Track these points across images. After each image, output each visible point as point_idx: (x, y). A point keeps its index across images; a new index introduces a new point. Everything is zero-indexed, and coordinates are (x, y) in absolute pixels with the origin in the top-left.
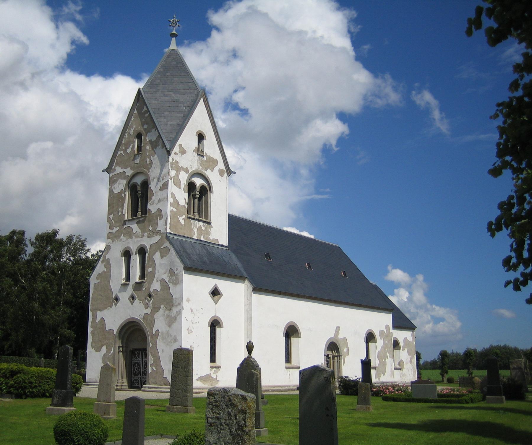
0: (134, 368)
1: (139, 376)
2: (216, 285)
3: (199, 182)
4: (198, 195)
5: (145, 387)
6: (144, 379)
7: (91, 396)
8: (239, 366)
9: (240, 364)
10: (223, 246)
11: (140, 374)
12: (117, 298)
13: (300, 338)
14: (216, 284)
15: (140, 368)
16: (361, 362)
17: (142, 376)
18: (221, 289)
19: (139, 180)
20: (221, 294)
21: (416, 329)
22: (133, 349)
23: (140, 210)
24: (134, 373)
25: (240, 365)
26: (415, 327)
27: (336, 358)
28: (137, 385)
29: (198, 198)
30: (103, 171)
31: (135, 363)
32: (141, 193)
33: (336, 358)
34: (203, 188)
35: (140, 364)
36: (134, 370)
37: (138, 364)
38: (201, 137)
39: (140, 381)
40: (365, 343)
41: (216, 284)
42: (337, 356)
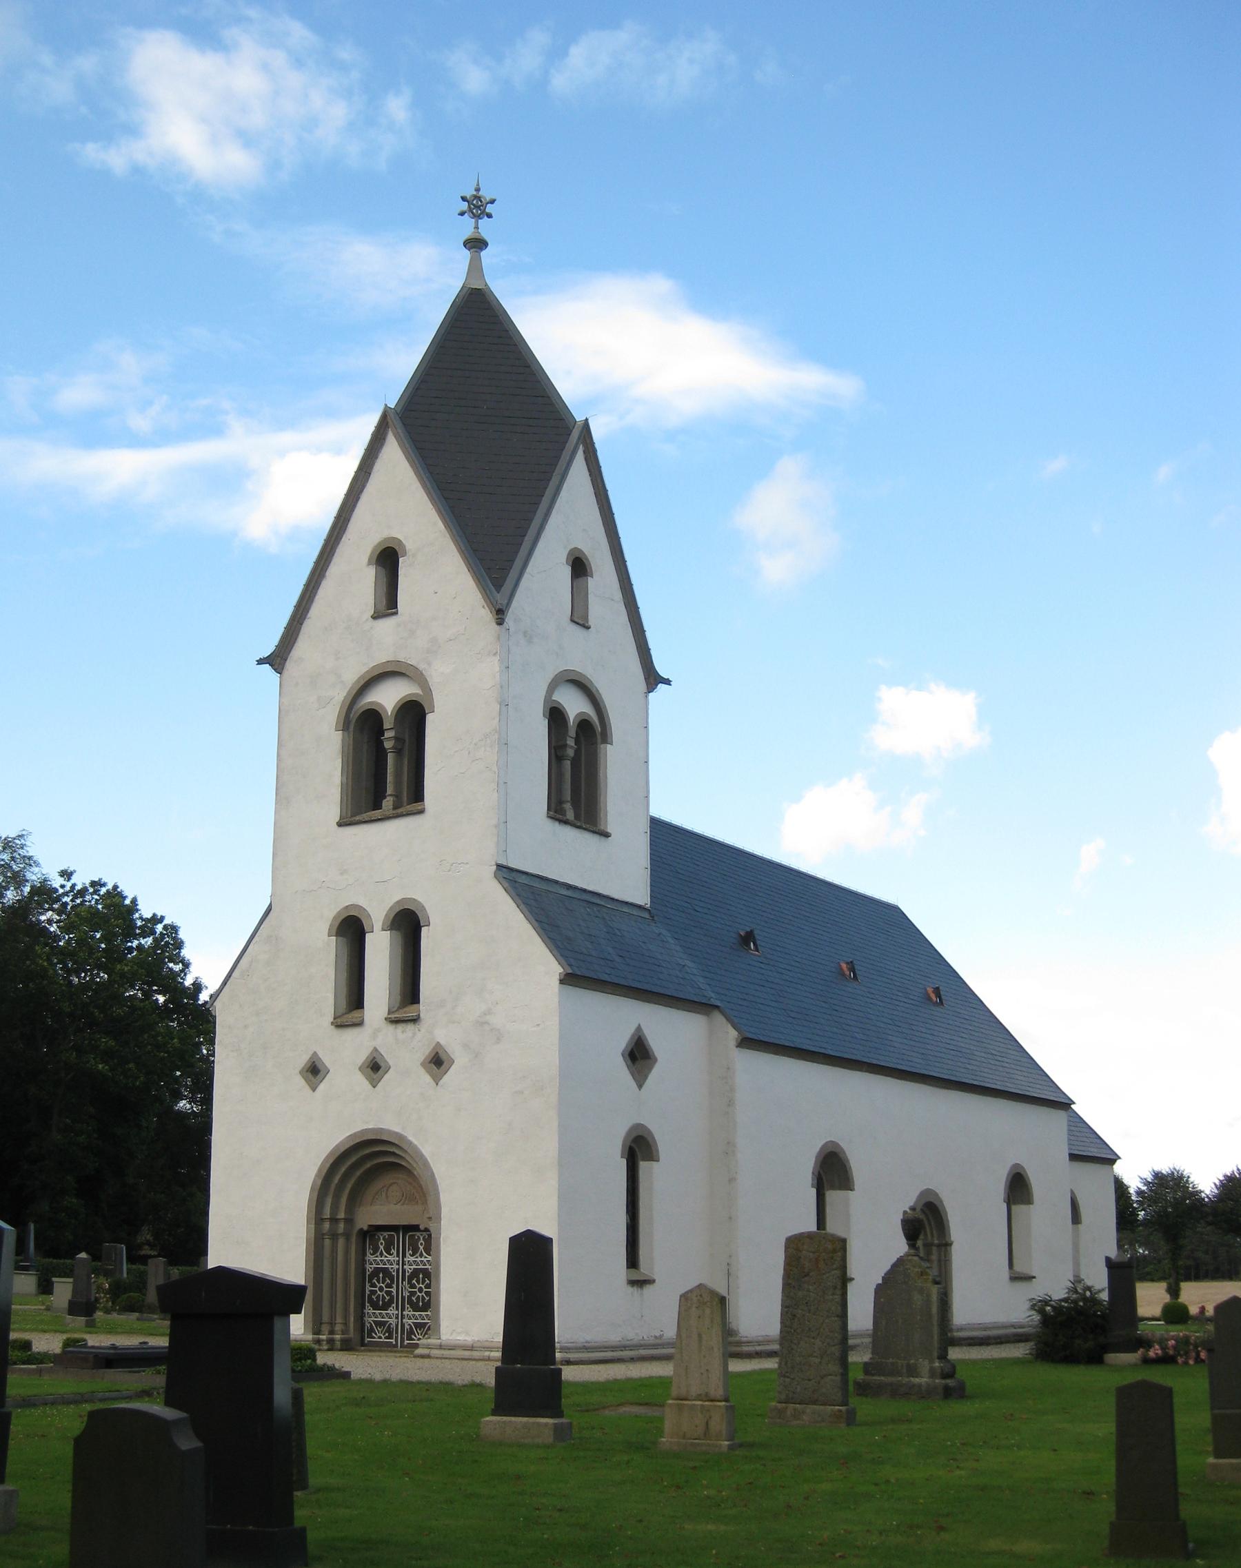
0: (373, 1285)
1: (392, 1311)
2: (641, 1029)
3: (575, 706)
4: (572, 747)
5: (428, 1347)
6: (410, 1319)
7: (580, 1378)
8: (880, 1282)
9: (883, 1275)
10: (639, 907)
11: (394, 1305)
12: (315, 1066)
13: (851, 1190)
14: (639, 1028)
15: (395, 1286)
16: (1107, 1266)
17: (403, 1309)
18: (655, 1043)
19: (388, 698)
20: (436, 1051)
21: (1118, 1161)
22: (370, 1226)
23: (390, 790)
24: (371, 1301)
25: (883, 1278)
26: (1116, 1154)
27: (934, 1249)
28: (386, 1338)
29: (573, 758)
30: (260, 662)
31: (376, 1272)
32: (396, 738)
33: (934, 1249)
34: (584, 725)
35: (395, 1274)
36: (373, 1292)
37: (386, 1272)
38: (579, 567)
39: (397, 1326)
40: (1005, 1205)
41: (639, 1028)
42: (939, 1246)
